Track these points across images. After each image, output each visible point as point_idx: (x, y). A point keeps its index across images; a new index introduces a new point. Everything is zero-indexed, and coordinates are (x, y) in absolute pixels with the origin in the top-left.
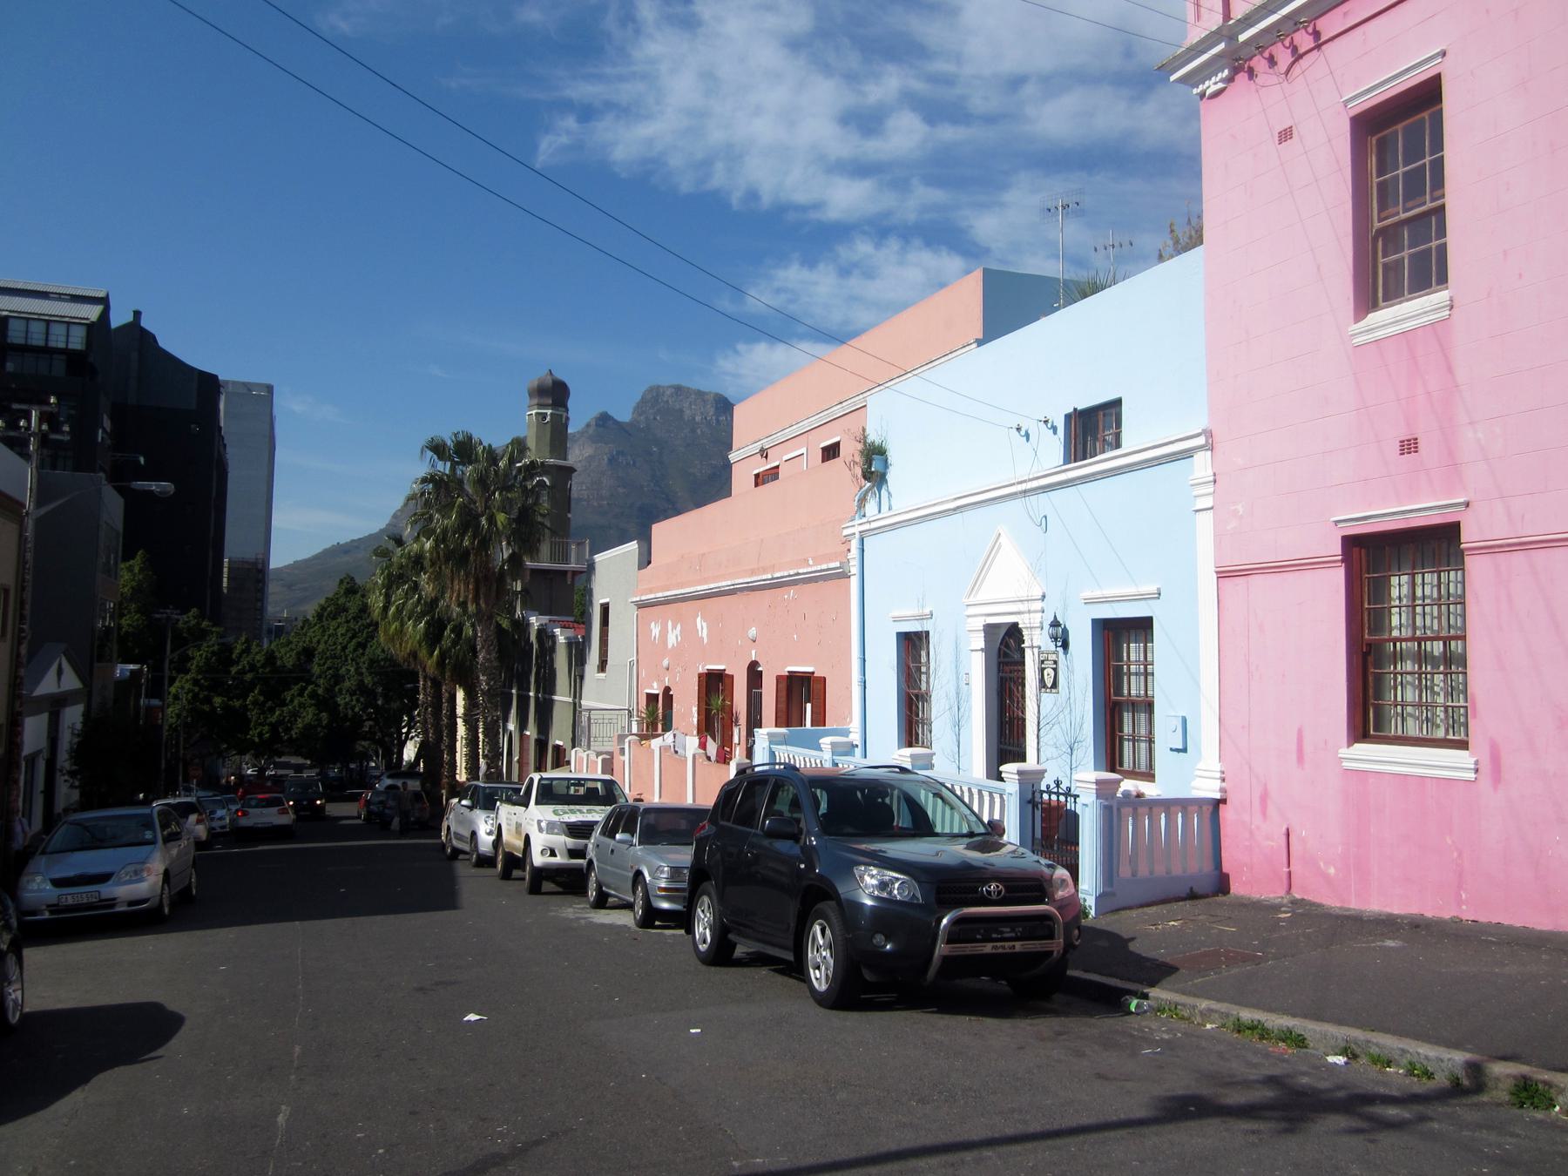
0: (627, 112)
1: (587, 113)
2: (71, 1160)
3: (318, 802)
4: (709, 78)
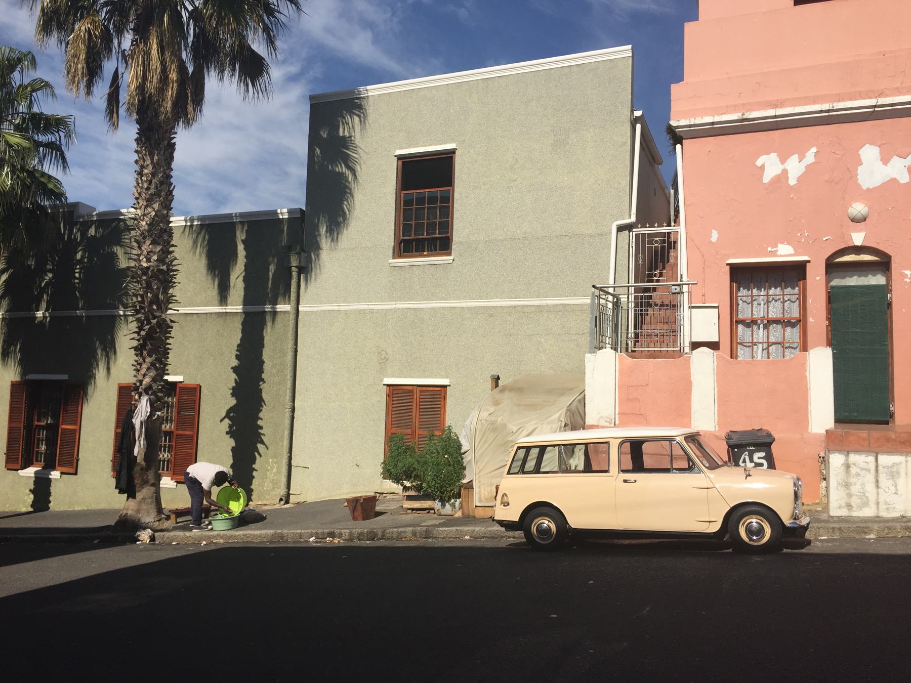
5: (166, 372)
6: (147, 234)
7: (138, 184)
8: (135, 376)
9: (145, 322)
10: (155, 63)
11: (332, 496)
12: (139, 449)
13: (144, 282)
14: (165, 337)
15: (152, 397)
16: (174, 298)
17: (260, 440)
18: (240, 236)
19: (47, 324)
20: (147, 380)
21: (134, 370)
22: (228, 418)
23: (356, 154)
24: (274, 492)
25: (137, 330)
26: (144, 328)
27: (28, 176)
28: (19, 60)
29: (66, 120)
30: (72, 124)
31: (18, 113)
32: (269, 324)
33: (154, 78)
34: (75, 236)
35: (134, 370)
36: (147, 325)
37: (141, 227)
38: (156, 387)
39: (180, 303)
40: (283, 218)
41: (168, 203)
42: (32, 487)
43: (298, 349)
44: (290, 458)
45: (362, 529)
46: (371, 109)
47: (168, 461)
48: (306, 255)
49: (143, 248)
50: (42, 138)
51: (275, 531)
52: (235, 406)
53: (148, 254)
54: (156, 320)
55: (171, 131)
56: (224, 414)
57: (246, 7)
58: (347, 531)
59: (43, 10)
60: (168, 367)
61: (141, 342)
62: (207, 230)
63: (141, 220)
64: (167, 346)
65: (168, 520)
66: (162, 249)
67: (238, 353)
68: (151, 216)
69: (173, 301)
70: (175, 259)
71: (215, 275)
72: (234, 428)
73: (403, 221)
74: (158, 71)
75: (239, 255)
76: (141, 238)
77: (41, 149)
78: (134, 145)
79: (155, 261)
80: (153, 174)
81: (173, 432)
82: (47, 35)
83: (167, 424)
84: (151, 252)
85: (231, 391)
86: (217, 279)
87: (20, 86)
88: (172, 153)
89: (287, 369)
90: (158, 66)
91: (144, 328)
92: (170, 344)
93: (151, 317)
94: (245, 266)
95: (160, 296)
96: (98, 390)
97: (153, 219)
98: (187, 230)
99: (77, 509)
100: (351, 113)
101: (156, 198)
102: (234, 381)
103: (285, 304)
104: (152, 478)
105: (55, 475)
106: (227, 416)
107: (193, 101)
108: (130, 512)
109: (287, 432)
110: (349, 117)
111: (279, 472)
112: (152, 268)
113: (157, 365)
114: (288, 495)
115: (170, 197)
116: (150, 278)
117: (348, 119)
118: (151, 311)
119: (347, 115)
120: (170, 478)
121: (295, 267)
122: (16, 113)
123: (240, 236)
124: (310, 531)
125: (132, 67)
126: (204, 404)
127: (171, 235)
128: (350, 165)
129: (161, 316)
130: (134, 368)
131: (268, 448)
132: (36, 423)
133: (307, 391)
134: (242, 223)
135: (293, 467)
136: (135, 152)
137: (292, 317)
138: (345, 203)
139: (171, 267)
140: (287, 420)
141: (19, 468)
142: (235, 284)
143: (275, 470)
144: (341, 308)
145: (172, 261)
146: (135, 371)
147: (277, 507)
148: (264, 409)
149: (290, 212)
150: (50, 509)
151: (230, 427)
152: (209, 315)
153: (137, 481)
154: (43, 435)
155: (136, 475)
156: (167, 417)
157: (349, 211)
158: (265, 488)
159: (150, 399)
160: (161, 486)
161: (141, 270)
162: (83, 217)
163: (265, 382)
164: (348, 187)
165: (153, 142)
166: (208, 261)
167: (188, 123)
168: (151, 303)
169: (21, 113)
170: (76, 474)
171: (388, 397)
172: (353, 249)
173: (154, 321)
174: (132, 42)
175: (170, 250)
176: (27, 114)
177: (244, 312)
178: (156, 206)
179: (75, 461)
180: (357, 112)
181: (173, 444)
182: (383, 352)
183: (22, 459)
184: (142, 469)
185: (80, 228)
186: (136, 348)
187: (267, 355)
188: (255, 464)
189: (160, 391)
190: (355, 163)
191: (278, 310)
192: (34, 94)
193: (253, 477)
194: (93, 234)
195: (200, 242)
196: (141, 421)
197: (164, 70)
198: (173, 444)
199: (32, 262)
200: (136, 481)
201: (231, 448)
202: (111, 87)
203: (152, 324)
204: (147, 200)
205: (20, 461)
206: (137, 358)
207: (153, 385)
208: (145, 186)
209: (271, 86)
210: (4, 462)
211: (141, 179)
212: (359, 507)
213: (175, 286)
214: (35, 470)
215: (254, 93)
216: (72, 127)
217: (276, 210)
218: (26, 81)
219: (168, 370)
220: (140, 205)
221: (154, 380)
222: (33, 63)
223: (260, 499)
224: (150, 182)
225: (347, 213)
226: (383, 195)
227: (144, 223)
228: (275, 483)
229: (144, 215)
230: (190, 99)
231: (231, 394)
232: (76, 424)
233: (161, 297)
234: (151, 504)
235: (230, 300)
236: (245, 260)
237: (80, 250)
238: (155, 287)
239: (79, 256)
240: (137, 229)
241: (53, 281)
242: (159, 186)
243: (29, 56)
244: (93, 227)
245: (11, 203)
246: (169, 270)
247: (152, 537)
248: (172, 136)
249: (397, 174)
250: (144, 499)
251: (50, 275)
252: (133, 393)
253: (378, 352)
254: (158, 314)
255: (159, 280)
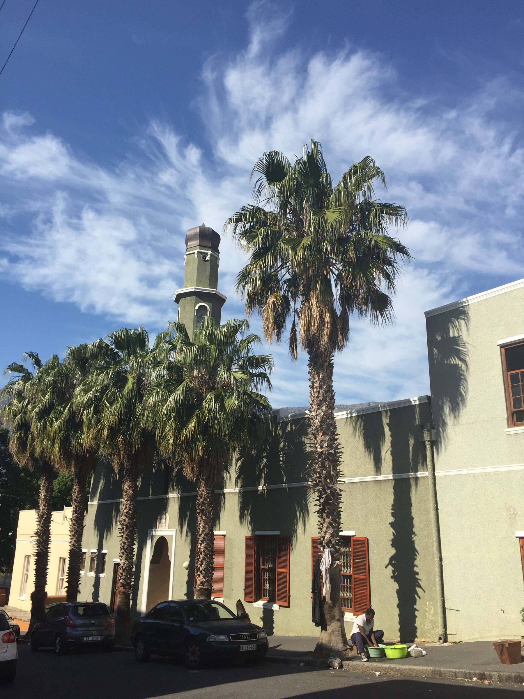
0: (34, 261)
1: (14, 259)
2: (303, 665)
3: (10, 534)
4: (82, 254)
5: (341, 529)
6: (319, 428)
7: (312, 395)
8: (319, 533)
9: (323, 492)
10: (316, 314)
11: (483, 638)
12: (326, 590)
13: (320, 462)
14: (337, 502)
15: (332, 549)
16: (341, 473)
17: (418, 584)
18: (386, 421)
19: (265, 494)
20: (327, 536)
21: (318, 528)
22: (391, 565)
23: (465, 348)
24: (434, 631)
25: (318, 498)
26: (322, 497)
27: (248, 397)
28: (240, 326)
29: (268, 357)
30: (272, 360)
31: (242, 357)
32: (413, 488)
33: (316, 323)
34: (279, 432)
35: (318, 528)
36: (325, 494)
37: (316, 424)
38: (334, 541)
39: (345, 476)
40: (415, 405)
41: (331, 405)
42: (262, 616)
43: (439, 507)
44: (443, 602)
45: (509, 673)
46: (472, 312)
47: (351, 600)
48: (436, 431)
49: (317, 439)
50: (255, 371)
51: (434, 668)
52: (395, 555)
53: (321, 442)
54: (330, 490)
55: (330, 356)
56: (387, 562)
57: (371, 265)
58: (496, 673)
59: (248, 295)
60: (341, 526)
61: (322, 507)
62: (362, 419)
63: (315, 419)
64: (339, 509)
65: (352, 651)
66: (330, 438)
67: (393, 512)
68: (321, 415)
69: (341, 475)
70: (340, 444)
71: (370, 451)
72: (397, 573)
73: (513, 397)
74: (318, 318)
75: (386, 436)
76: (316, 431)
77: (255, 378)
78: (308, 369)
79: (327, 447)
80: (320, 387)
81: (351, 576)
82: (252, 310)
83: (348, 570)
84: (323, 441)
85: (391, 543)
86: (372, 454)
87: (242, 340)
88: (332, 370)
89: (432, 525)
90: (317, 315)
91: (322, 497)
92: (341, 508)
93: (326, 488)
94: (391, 443)
95: (331, 472)
96: (299, 541)
97: (322, 417)
98: (349, 420)
99: (291, 635)
100: (457, 318)
101: (323, 403)
102: (392, 535)
103: (424, 471)
104: (337, 615)
105: (275, 607)
106: (390, 563)
107: (342, 334)
108: (324, 642)
109: (438, 579)
110: (456, 321)
111: (435, 614)
112: (324, 452)
113: (334, 524)
114: (445, 635)
115: (332, 401)
116: (324, 459)
117: (456, 323)
118: (326, 484)
119: (455, 320)
120: (352, 614)
121: (428, 441)
122: (240, 358)
123: (386, 421)
124: (463, 671)
125: (301, 319)
126: (371, 554)
127: (335, 428)
128: (462, 357)
129: (333, 487)
130: (318, 526)
131: (424, 592)
132: (262, 567)
133: (450, 543)
134: (386, 411)
135: (447, 610)
136: (308, 373)
137: (430, 481)
138: (461, 387)
139: (337, 450)
140: (437, 568)
141: (253, 601)
142: (385, 458)
143: (432, 612)
144: (469, 472)
145: (337, 446)
146: (319, 529)
147: (437, 644)
148: (418, 557)
149: (420, 399)
150: (274, 634)
151: (394, 572)
152: (368, 483)
153: (327, 617)
154: (267, 577)
155: (326, 612)
156: (347, 563)
157: (465, 392)
158: (426, 627)
159: (330, 550)
160: (345, 619)
161: (317, 454)
162: (283, 418)
163: (416, 535)
164: (463, 375)
165: (319, 365)
166: (365, 441)
167: (340, 348)
168: (326, 478)
169: (243, 357)
170: (289, 607)
171: (522, 548)
172: (473, 423)
173: (329, 491)
174: (302, 303)
175: (335, 438)
176: (246, 357)
177: (394, 479)
178: (324, 408)
179: (288, 597)
180: (463, 317)
181: (353, 585)
182: (511, 508)
183: (254, 594)
184: (330, 607)
185: (281, 426)
186: (318, 512)
187: (415, 512)
188: (416, 604)
189: (337, 544)
190: (466, 355)
191: (419, 476)
192: (249, 344)
193: (416, 617)
194: (290, 430)
195: (358, 427)
196: (326, 568)
197: (321, 317)
198: (353, 585)
199: (254, 452)
200: (326, 616)
201: (396, 590)
202: (291, 334)
203: (328, 494)
204: (318, 405)
205: (253, 596)
206: (319, 519)
207: (332, 540)
208: (316, 395)
209: (394, 314)
210: (244, 596)
211: (313, 391)
212: (505, 652)
213: (341, 464)
214: (264, 603)
215: (383, 321)
216: (272, 362)
217: (410, 399)
218: (244, 338)
219: (341, 528)
220: (314, 408)
221: (332, 536)
222: (248, 325)
223: (422, 637)
224: (319, 392)
225: (464, 395)
226: (492, 377)
227: (317, 421)
228: (434, 623)
229: (317, 415)
230: (339, 332)
231: (391, 545)
232: (287, 568)
233: (332, 473)
234: (338, 636)
235: (383, 469)
236: (390, 438)
237: (282, 442)
238: (328, 466)
239: (282, 445)
240: (313, 426)
241: (268, 464)
242: (324, 394)
243: (246, 322)
244: (289, 426)
245: (238, 416)
246: (336, 453)
247: (340, 664)
248: (331, 359)
249: (501, 359)
250: (333, 632)
251: (265, 460)
252: (319, 546)
253: (506, 508)
254: (331, 486)
255: (330, 460)
